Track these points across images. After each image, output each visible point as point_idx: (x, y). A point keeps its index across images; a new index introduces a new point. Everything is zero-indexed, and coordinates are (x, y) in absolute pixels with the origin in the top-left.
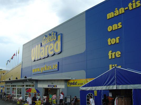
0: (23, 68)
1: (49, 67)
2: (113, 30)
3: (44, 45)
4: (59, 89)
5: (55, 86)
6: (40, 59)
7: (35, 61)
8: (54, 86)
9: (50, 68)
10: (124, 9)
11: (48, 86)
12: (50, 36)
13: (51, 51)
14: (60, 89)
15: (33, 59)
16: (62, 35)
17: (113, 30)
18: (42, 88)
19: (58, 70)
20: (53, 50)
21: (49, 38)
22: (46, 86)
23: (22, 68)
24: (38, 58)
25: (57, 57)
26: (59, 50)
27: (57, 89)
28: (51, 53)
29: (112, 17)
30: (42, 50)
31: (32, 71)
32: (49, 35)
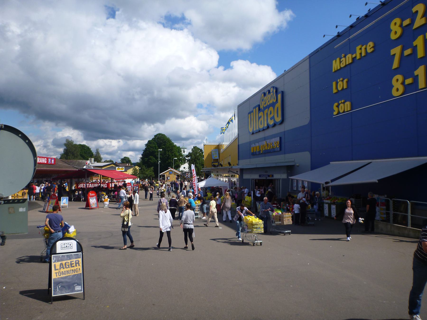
0: (240, 144)
1: (269, 144)
2: (344, 88)
3: (263, 109)
4: (277, 179)
5: (271, 176)
6: (259, 131)
7: (253, 133)
8: (269, 176)
9: (271, 146)
10: (352, 57)
11: (260, 176)
12: (265, 97)
13: (271, 119)
14: (279, 180)
15: (251, 131)
16: (221, 128)
17: (344, 88)
18: (250, 179)
19: (281, 149)
20: (273, 118)
21: (267, 98)
22: (256, 176)
23: (238, 145)
24: (256, 129)
25: (278, 130)
26: (278, 119)
27: (275, 179)
28: (271, 123)
29: (350, 62)
30: (261, 117)
31: (250, 150)
32: (267, 92)
